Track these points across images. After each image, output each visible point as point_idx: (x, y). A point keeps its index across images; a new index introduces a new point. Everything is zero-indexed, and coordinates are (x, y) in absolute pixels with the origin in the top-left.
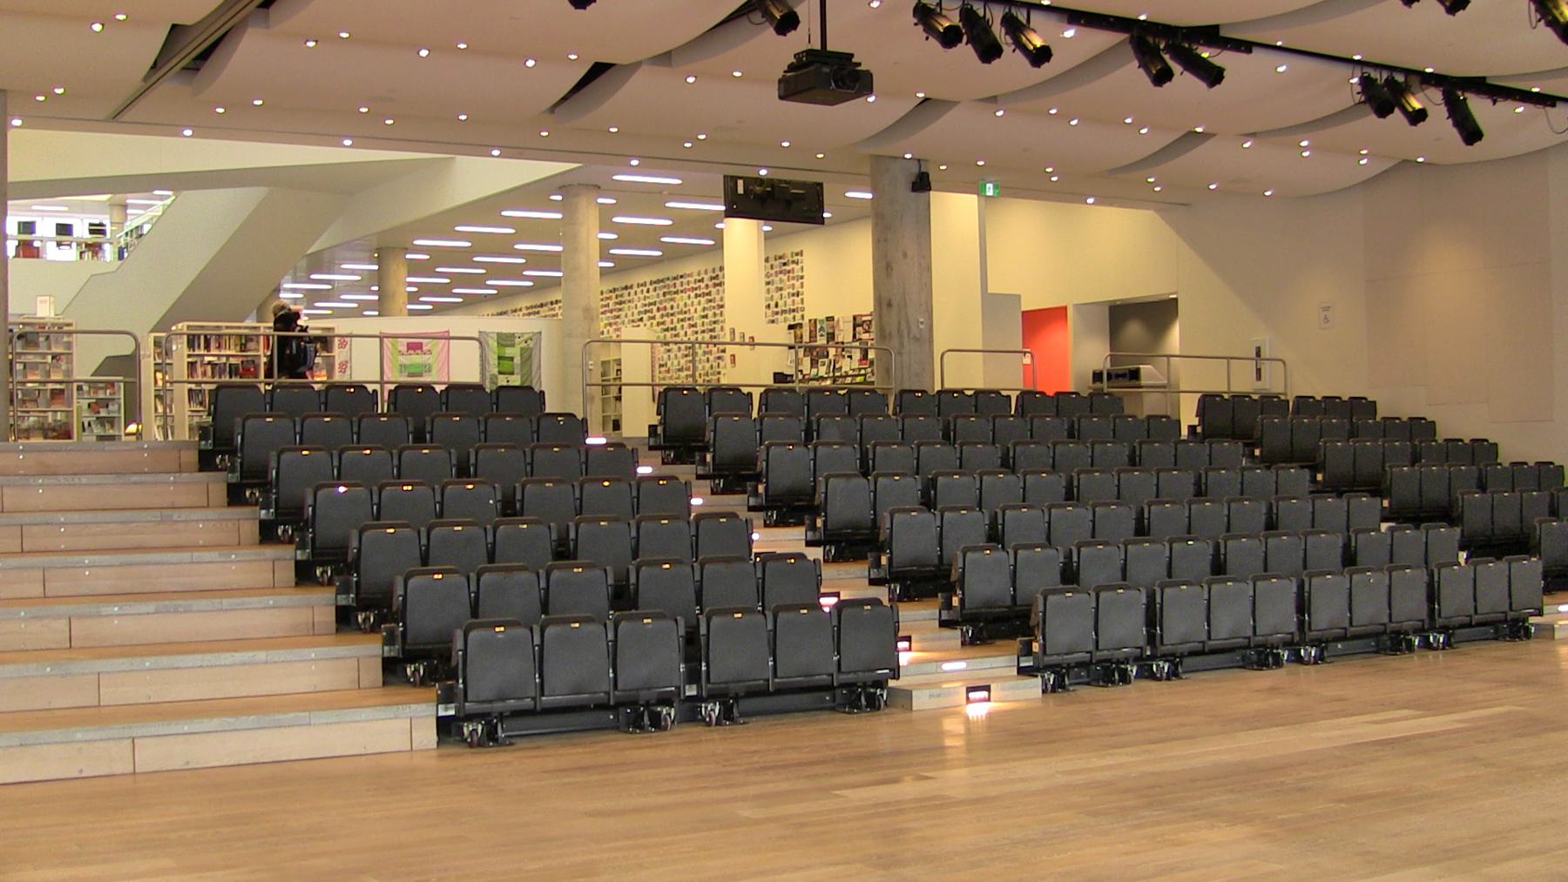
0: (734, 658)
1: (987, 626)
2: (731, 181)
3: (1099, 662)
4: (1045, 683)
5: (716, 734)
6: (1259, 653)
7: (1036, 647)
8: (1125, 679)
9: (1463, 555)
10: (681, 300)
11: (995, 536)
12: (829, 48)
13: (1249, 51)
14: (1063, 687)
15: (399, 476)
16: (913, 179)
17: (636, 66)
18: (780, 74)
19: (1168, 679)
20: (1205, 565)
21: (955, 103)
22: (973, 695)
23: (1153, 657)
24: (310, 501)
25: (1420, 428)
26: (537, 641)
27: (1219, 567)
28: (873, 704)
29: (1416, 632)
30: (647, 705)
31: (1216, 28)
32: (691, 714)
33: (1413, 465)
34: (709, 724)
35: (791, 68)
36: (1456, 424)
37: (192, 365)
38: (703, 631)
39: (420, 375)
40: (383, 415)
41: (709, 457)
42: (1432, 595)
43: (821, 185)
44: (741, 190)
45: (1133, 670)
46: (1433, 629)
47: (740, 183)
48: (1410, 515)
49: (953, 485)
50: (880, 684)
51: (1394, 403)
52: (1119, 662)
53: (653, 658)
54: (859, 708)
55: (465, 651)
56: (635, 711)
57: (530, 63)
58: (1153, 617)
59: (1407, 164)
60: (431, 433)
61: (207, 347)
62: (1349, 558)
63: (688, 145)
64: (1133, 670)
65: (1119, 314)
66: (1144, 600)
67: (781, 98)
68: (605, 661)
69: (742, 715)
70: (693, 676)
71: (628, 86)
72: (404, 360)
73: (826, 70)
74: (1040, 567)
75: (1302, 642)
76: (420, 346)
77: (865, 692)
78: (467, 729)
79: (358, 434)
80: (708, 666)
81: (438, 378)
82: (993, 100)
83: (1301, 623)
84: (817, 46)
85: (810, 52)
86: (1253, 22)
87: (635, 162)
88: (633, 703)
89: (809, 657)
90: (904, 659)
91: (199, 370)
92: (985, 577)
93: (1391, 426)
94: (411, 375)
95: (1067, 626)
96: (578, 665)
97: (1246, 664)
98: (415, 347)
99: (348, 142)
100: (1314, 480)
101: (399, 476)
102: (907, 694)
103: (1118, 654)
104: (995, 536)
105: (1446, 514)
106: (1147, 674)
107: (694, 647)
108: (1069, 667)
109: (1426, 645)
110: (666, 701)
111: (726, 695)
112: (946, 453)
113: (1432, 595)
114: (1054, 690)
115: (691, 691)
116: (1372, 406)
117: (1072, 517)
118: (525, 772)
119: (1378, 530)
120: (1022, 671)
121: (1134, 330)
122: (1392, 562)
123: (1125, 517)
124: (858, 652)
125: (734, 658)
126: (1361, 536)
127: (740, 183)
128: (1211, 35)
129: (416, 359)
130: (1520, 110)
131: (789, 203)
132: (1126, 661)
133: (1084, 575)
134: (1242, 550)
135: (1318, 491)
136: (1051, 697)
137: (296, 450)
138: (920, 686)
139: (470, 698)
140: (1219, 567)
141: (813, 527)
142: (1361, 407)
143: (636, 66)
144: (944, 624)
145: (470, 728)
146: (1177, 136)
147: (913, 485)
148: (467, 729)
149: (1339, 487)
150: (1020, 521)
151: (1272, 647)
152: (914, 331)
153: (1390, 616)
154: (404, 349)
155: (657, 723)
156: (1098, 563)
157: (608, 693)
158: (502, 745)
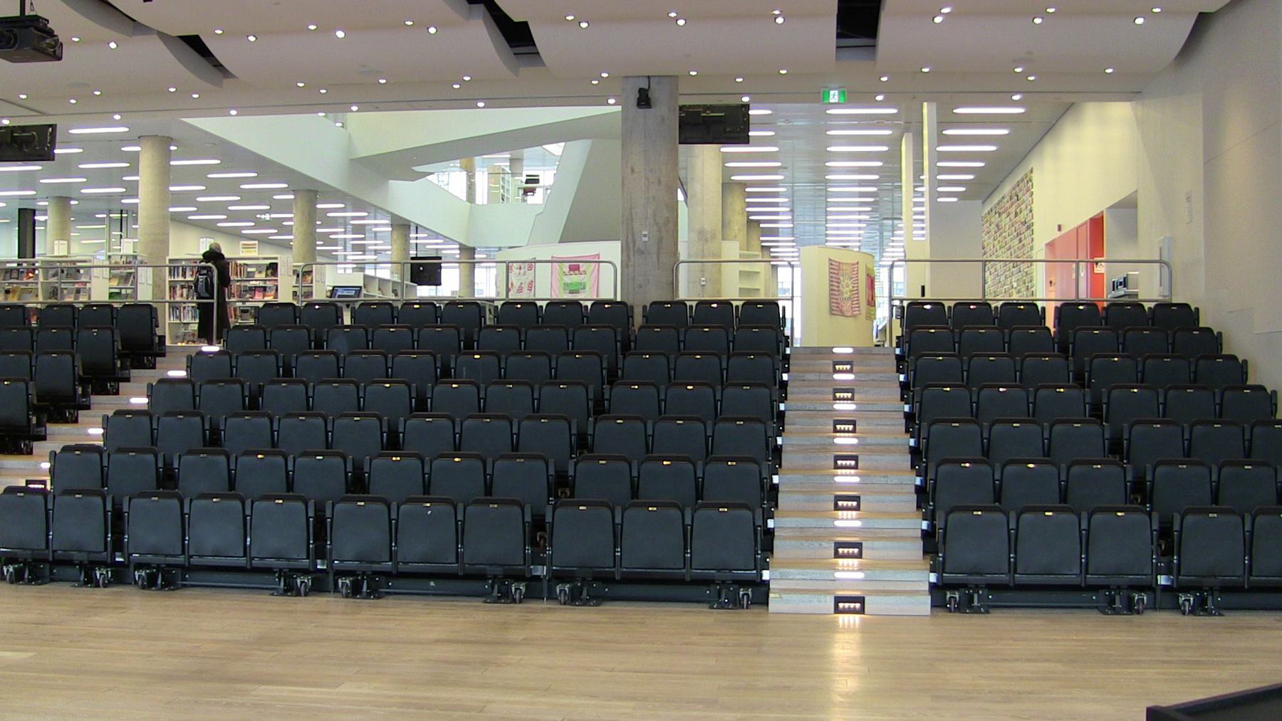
5: (1189, 619)
15: (1195, 381)
21: (181, 37)
37: (173, 288)
39: (577, 292)
40: (347, 327)
53: (498, 538)
55: (945, 529)
56: (1202, 594)
57: (432, 30)
60: (1073, 344)
61: (184, 275)
63: (456, 86)
72: (567, 279)
76: (578, 268)
79: (1124, 344)
80: (1179, 560)
81: (587, 297)
87: (880, 98)
91: (179, 292)
94: (571, 292)
96: (498, 538)
98: (575, 268)
99: (481, 104)
101: (1195, 381)
129: (575, 278)
137: (571, 354)
139: (1091, 570)
154: (567, 270)
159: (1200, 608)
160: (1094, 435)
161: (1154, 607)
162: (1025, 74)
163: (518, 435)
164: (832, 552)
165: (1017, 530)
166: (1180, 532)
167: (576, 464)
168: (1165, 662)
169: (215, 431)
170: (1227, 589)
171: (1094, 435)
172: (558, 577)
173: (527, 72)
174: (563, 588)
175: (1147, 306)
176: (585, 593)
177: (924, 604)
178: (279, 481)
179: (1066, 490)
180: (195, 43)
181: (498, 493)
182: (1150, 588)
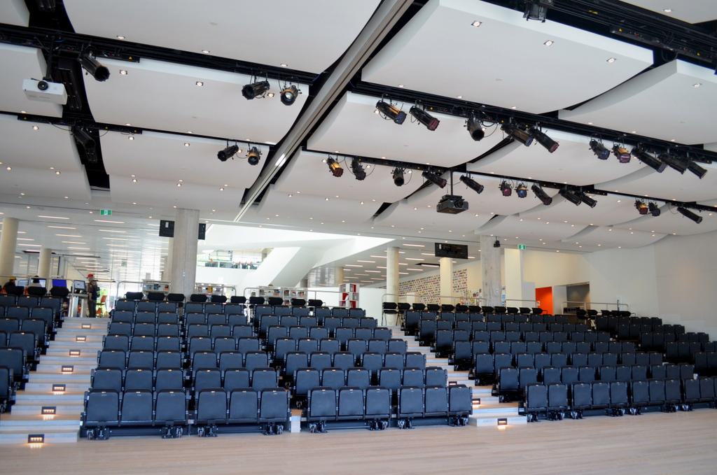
0: (411, 402)
1: (509, 395)
2: (437, 245)
3: (550, 411)
4: (529, 418)
6: (613, 410)
7: (525, 405)
8: (560, 418)
9: (696, 376)
10: (429, 285)
11: (514, 364)
12: (454, 194)
13: (606, 195)
14: (536, 420)
16: (494, 243)
17: (397, 203)
18: (437, 203)
19: (577, 418)
20: (592, 376)
21: (506, 216)
22: (500, 422)
23: (571, 410)
24: (275, 343)
25: (678, 329)
26: (365, 395)
27: (598, 377)
28: (462, 424)
29: (677, 404)
30: (459, 417)
31: (593, 186)
32: (395, 424)
33: (675, 341)
34: (400, 428)
35: (441, 201)
36: (692, 327)
38: (399, 394)
41: (419, 333)
42: (683, 390)
43: (466, 246)
44: (440, 248)
45: (563, 415)
46: (684, 403)
47: (440, 245)
48: (674, 359)
49: (501, 345)
50: (466, 416)
51: (669, 319)
52: (557, 412)
54: (457, 425)
55: (311, 398)
58: (570, 395)
59: (670, 235)
62: (649, 375)
64: (563, 415)
65: (571, 289)
66: (567, 388)
67: (438, 211)
68: (446, 401)
69: (584, 416)
70: (395, 411)
71: (396, 210)
73: (452, 201)
74: (530, 374)
75: (630, 407)
77: (457, 418)
78: (311, 426)
82: (518, 214)
83: (629, 399)
84: (450, 194)
85: (446, 196)
86: (350, 46)
88: (454, 416)
89: (437, 403)
90: (474, 406)
92: (508, 377)
93: (667, 328)
95: (537, 395)
97: (608, 414)
100: (637, 346)
102: (474, 420)
103: (557, 409)
104: (514, 364)
105: (689, 359)
106: (568, 416)
107: (395, 400)
108: (538, 413)
109: (681, 409)
110: (386, 419)
111: (455, 416)
112: (501, 335)
113: (683, 390)
114: (532, 421)
115: (394, 416)
116: (660, 321)
117: (544, 358)
118: (545, 425)
119: (661, 365)
120: (521, 414)
121: (575, 294)
122: (667, 377)
123: (563, 359)
124: (456, 405)
125: (211, 405)
126: (479, 356)
127: (440, 245)
128: (590, 188)
130: (710, 214)
131: (456, 252)
132: (561, 411)
133: (546, 378)
134: (608, 371)
135: (640, 350)
136: (530, 423)
138: (479, 418)
139: (402, 412)
140: (598, 377)
141: (451, 358)
142: (656, 321)
143: (397, 203)
144: (493, 395)
145: (535, 415)
146: (584, 228)
147: (486, 346)
148: (311, 426)
149: (646, 349)
150: (524, 359)
151: (618, 408)
152: (495, 293)
153: (650, 399)
155: (381, 427)
156: (551, 374)
157: (446, 412)
158: (323, 432)
159: (207, 434)
160: (266, 359)
161: (185, 433)
162: (579, 245)
163: (157, 359)
164: (41, 411)
165: (122, 400)
166: (311, 398)
167: (126, 371)
168: (458, 445)
169: (358, 359)
170: (219, 425)
171: (266, 359)
172: (199, 425)
173: (100, 194)
174: (402, 423)
175: (330, 308)
176: (211, 431)
177: (74, 438)
178: (217, 383)
179: (156, 381)
180: (669, 235)
181: (325, 384)
182: (184, 425)
